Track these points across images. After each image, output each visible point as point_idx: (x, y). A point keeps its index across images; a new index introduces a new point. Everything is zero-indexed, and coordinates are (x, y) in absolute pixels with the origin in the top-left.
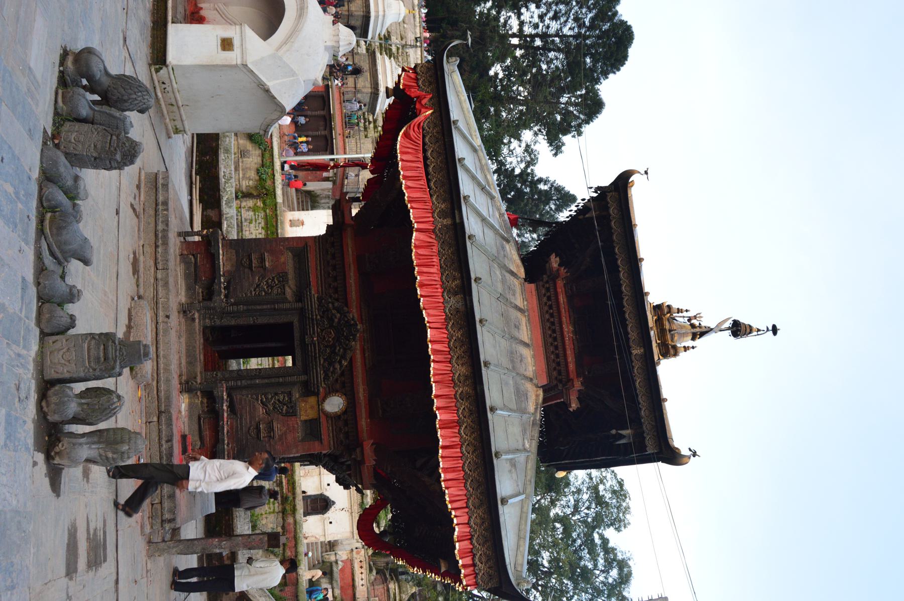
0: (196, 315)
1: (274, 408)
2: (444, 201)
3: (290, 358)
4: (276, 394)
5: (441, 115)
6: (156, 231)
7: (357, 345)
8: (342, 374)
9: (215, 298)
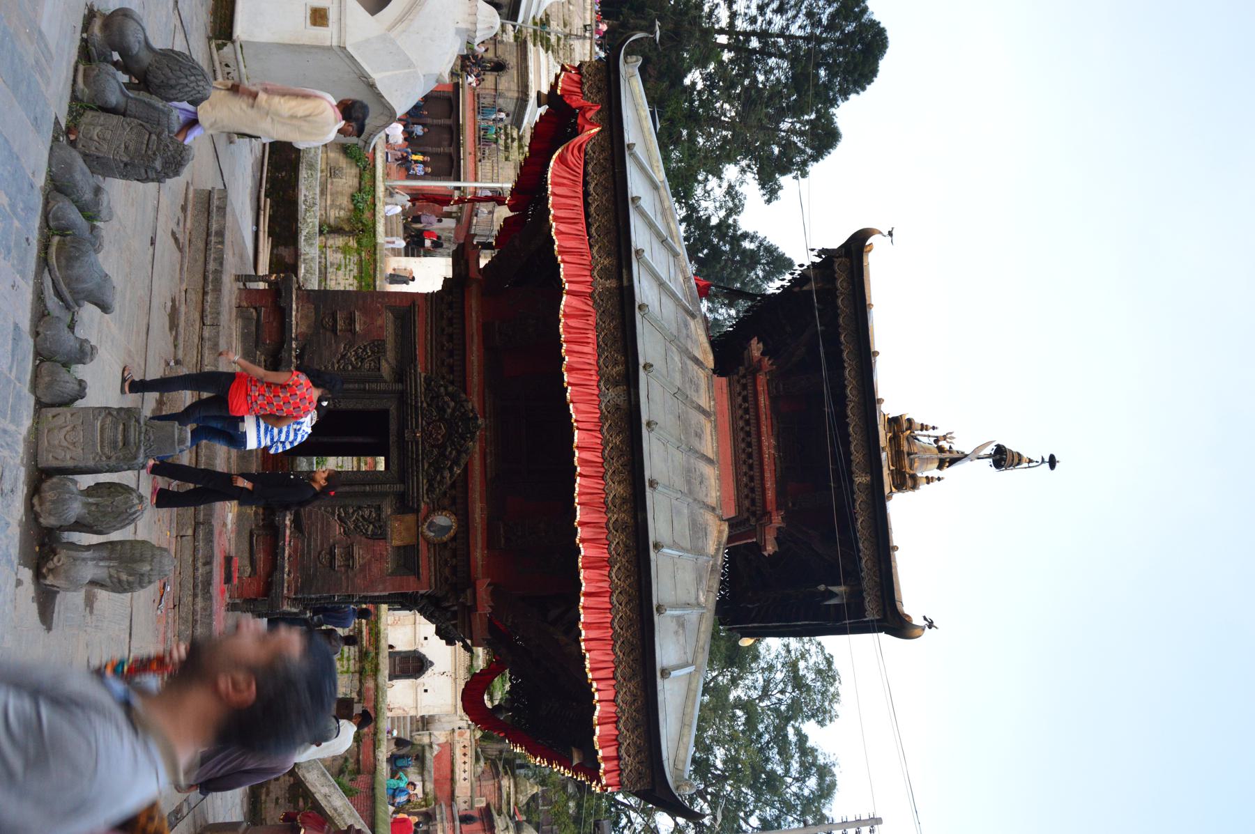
2: (608, 255)
4: (360, 508)
7: (475, 447)
8: (453, 485)
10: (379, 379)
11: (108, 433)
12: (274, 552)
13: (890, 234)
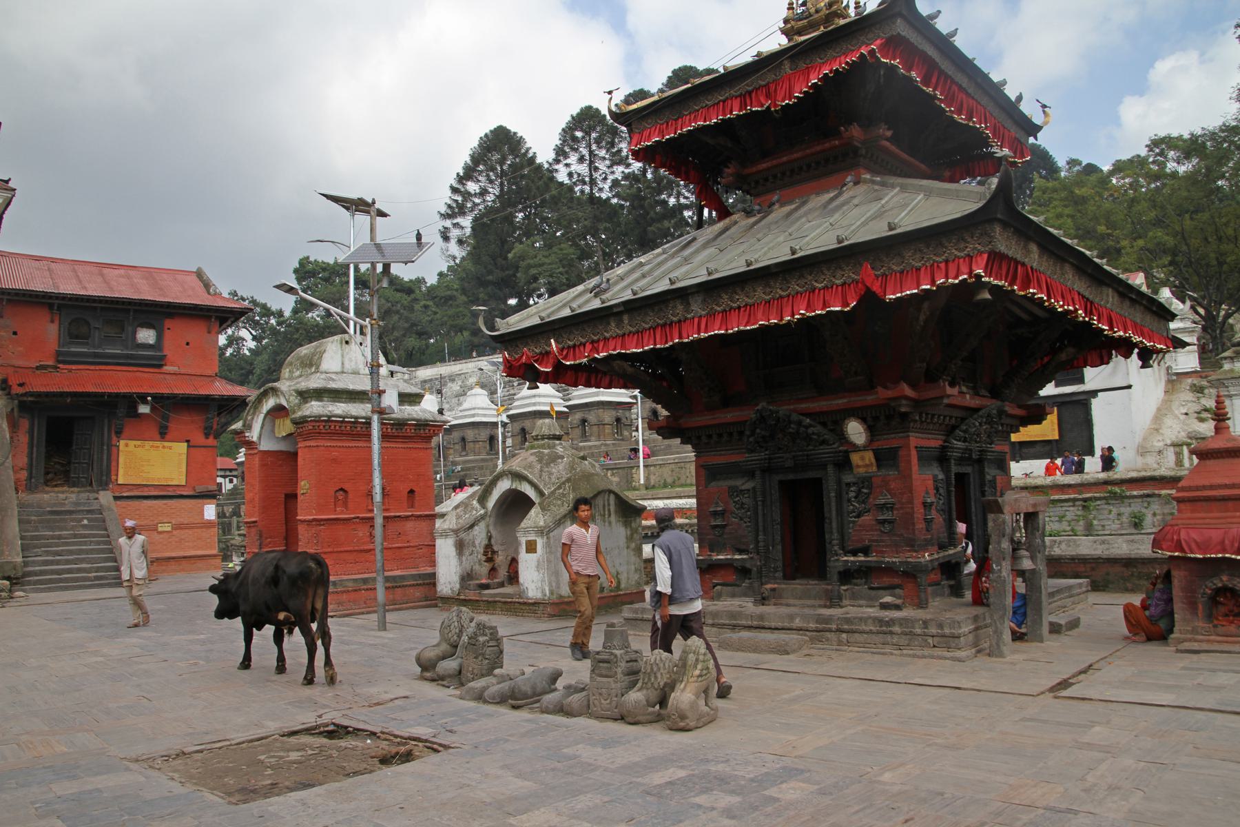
0: (769, 586)
1: (864, 502)
2: (609, 324)
3: (1018, 469)
4: (849, 500)
5: (541, 333)
6: (878, 633)
7: (783, 410)
8: (824, 424)
9: (748, 565)
10: (754, 488)
11: (604, 672)
12: (890, 570)
13: (610, 93)
